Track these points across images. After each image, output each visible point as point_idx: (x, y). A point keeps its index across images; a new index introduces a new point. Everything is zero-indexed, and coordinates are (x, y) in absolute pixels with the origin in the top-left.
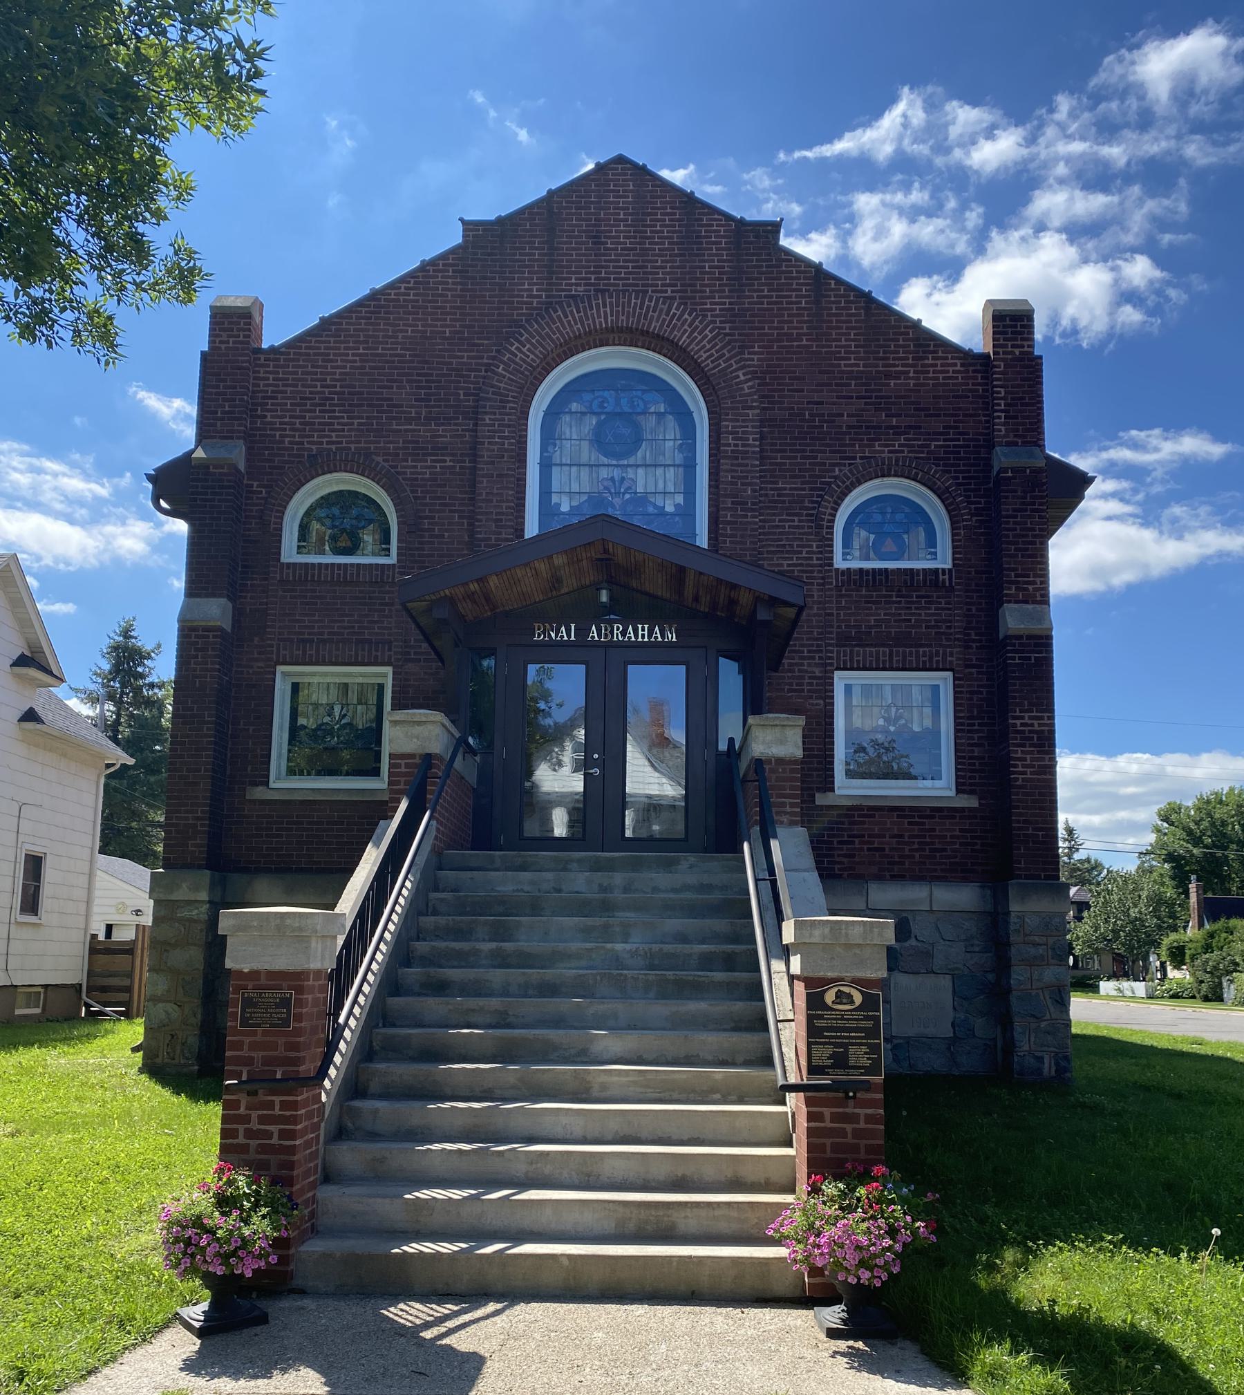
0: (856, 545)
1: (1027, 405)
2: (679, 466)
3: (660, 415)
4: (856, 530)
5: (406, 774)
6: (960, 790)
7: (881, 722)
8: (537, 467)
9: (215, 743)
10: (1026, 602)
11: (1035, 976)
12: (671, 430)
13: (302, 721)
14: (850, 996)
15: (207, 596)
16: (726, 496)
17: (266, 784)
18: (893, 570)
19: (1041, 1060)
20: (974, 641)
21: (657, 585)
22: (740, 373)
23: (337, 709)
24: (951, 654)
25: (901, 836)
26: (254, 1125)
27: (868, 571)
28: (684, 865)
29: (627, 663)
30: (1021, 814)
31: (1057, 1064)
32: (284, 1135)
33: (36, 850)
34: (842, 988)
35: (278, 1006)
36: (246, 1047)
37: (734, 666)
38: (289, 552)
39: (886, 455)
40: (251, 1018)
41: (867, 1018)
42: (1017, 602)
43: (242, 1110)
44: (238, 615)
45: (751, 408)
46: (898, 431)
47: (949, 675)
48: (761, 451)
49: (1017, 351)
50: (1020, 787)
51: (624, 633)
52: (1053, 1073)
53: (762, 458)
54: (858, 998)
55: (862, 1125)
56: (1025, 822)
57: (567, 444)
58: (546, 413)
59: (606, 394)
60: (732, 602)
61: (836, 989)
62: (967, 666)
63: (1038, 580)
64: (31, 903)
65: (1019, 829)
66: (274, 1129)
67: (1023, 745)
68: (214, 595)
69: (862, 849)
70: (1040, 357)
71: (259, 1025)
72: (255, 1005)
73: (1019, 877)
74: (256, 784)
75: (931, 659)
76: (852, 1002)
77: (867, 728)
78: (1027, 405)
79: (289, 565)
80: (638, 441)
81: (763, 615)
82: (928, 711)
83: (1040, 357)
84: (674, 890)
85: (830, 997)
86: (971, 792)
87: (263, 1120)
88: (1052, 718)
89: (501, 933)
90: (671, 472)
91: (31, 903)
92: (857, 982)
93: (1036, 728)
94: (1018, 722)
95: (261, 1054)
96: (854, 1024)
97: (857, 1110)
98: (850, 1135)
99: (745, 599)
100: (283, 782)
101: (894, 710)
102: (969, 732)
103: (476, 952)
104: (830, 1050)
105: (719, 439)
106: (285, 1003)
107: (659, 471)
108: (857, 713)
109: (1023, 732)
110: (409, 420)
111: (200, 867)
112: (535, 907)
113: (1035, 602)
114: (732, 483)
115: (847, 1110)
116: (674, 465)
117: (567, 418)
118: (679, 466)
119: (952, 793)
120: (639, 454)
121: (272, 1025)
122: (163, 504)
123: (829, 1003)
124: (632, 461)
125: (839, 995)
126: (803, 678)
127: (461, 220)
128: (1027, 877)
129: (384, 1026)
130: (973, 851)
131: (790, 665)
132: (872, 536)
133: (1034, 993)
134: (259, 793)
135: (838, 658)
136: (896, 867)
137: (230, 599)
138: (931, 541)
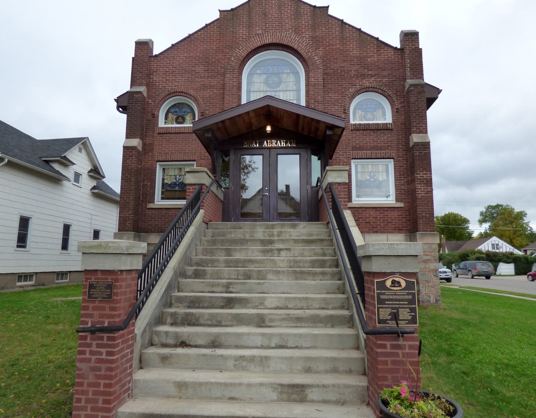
0: (357, 116)
1: (417, 65)
2: (294, 90)
3: (288, 73)
4: (358, 111)
5: (192, 192)
6: (397, 200)
7: (368, 177)
8: (246, 92)
9: (135, 188)
10: (420, 133)
11: (427, 267)
12: (292, 78)
13: (166, 181)
14: (399, 283)
15: (133, 138)
16: (312, 99)
17: (154, 202)
18: (371, 124)
19: (430, 297)
20: (401, 148)
21: (287, 124)
22: (316, 57)
23: (178, 177)
24: (393, 153)
25: (377, 218)
26: (94, 348)
27: (362, 124)
28: (301, 226)
29: (278, 154)
30: (420, 209)
31: (436, 298)
32: (109, 354)
33: (97, 228)
34: (395, 279)
35: (106, 288)
36: (90, 309)
37: (316, 158)
38: (161, 124)
39: (367, 84)
40: (93, 294)
41: (408, 294)
42: (417, 133)
43: (88, 341)
44: (144, 145)
45: (320, 69)
46: (371, 76)
47: (392, 160)
48: (324, 84)
49: (413, 47)
50: (419, 199)
51: (276, 143)
52: (434, 302)
53: (324, 86)
54: (403, 284)
55: (407, 351)
56: (422, 211)
57: (256, 84)
58: (249, 74)
59: (269, 67)
60: (317, 129)
61: (391, 279)
62: (398, 157)
63: (424, 125)
64: (22, 240)
65: (420, 214)
66: (104, 350)
67: (421, 184)
68: (135, 138)
69: (362, 223)
70: (421, 49)
71: (96, 298)
72: (95, 288)
73: (420, 231)
74: (149, 202)
75: (386, 155)
76: (400, 286)
77: (363, 180)
78: (417, 65)
79: (161, 128)
80: (280, 82)
81: (329, 132)
82: (385, 174)
83: (421, 49)
84: (298, 236)
85: (388, 283)
86: (401, 201)
87: (98, 346)
88: (431, 174)
89: (228, 252)
90: (292, 93)
91: (22, 240)
92: (403, 274)
93: (425, 177)
94: (419, 176)
95: (98, 312)
96: (401, 297)
97: (405, 343)
98: (401, 356)
99: (322, 128)
100: (159, 202)
101: (372, 173)
102: (400, 180)
103: (218, 261)
104: (389, 311)
105: (309, 80)
106: (110, 287)
107: (288, 92)
108: (359, 174)
109: (420, 179)
110: (201, 77)
111: (131, 231)
112: (243, 242)
113: (423, 133)
114: (313, 95)
115: (399, 343)
116: (293, 90)
117: (256, 76)
118: (294, 90)
119: (394, 202)
120: (281, 87)
121: (103, 298)
122: (120, 109)
123: (389, 287)
124: (278, 89)
125: (393, 282)
126: (340, 162)
127: (219, 10)
128: (423, 231)
129: (178, 292)
130: (402, 222)
131: (336, 158)
132: (363, 113)
133: (426, 273)
134: (151, 206)
135: (353, 156)
136: (375, 229)
137: (140, 139)
138: (384, 114)
